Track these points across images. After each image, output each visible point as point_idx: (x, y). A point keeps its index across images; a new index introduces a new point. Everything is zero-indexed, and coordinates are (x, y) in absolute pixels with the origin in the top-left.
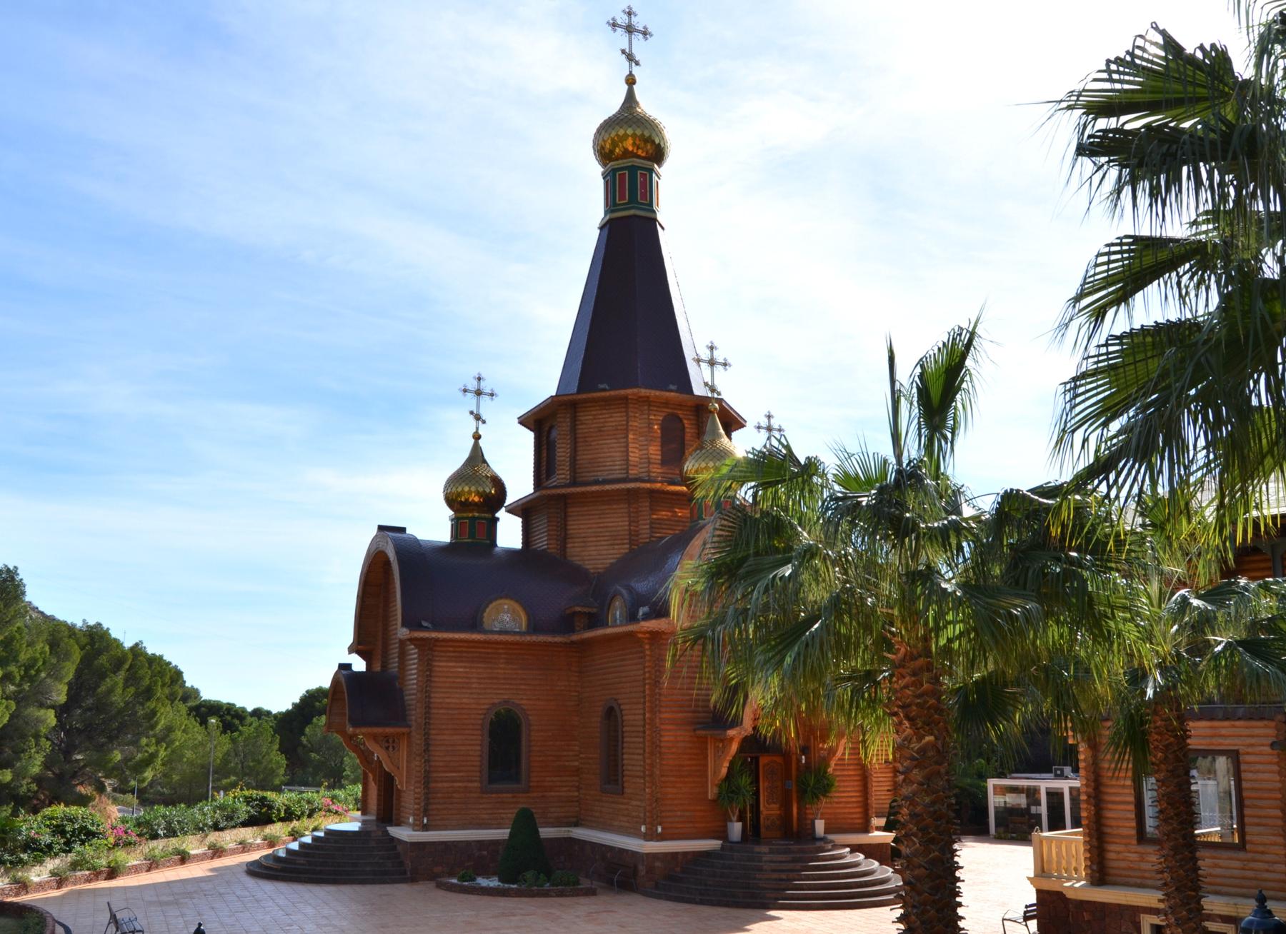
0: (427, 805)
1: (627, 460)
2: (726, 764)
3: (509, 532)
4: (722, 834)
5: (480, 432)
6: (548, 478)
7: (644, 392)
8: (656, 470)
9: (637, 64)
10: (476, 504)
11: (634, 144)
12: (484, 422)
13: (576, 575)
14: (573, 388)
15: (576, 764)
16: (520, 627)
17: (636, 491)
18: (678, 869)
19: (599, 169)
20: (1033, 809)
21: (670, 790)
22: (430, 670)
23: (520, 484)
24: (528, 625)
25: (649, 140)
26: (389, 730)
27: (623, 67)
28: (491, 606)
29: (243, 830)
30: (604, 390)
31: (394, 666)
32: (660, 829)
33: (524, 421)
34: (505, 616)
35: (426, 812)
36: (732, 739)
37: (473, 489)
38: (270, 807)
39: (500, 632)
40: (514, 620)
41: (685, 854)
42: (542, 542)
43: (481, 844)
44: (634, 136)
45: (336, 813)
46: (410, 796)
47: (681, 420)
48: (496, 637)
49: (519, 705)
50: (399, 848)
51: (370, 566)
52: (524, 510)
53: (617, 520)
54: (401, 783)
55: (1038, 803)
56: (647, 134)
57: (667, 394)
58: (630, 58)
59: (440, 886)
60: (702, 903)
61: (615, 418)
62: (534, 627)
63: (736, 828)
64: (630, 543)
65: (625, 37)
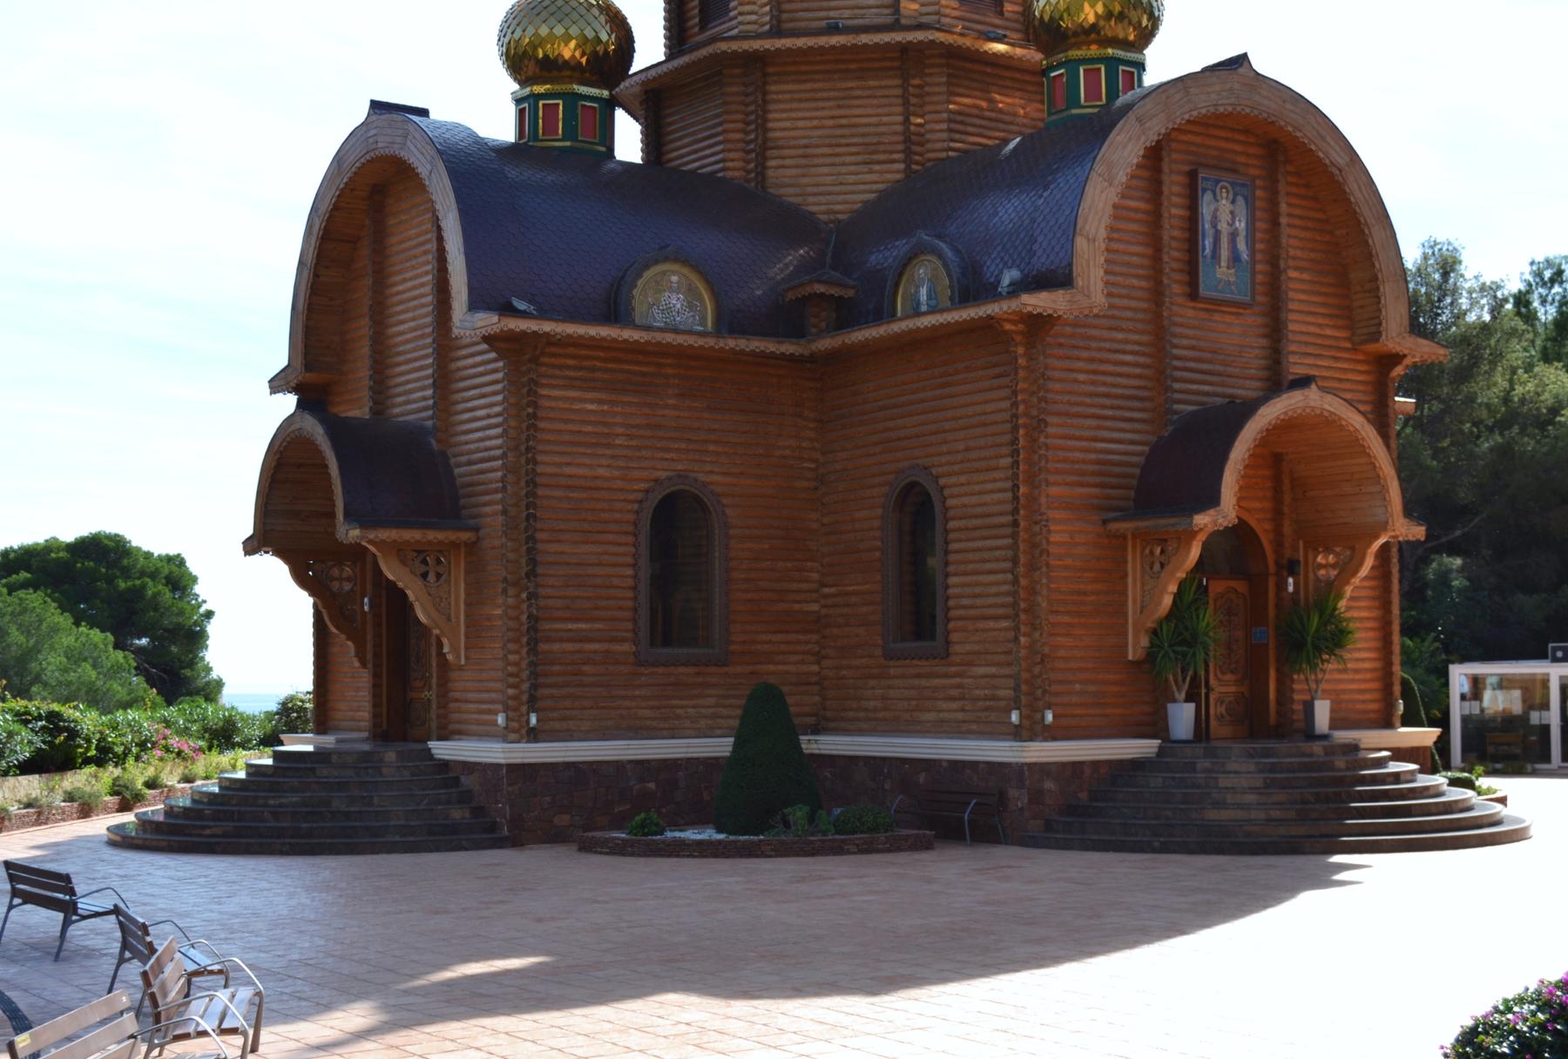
0: (535, 687)
2: (1173, 588)
4: (1156, 726)
6: (703, 26)
13: (790, 223)
15: (814, 607)
16: (703, 322)
18: (1084, 796)
20: (1535, 718)
21: (1061, 640)
22: (535, 405)
24: (718, 319)
26: (432, 535)
28: (648, 274)
29: (23, 779)
32: (1049, 717)
34: (672, 302)
35: (533, 703)
36: (1192, 534)
37: (574, 31)
38: (73, 734)
40: (691, 307)
41: (1096, 764)
42: (708, 151)
43: (644, 767)
49: (705, 484)
53: (876, 111)
55: (1545, 706)
59: (587, 847)
60: (1166, 849)
62: (729, 322)
63: (1182, 717)
64: (908, 161)
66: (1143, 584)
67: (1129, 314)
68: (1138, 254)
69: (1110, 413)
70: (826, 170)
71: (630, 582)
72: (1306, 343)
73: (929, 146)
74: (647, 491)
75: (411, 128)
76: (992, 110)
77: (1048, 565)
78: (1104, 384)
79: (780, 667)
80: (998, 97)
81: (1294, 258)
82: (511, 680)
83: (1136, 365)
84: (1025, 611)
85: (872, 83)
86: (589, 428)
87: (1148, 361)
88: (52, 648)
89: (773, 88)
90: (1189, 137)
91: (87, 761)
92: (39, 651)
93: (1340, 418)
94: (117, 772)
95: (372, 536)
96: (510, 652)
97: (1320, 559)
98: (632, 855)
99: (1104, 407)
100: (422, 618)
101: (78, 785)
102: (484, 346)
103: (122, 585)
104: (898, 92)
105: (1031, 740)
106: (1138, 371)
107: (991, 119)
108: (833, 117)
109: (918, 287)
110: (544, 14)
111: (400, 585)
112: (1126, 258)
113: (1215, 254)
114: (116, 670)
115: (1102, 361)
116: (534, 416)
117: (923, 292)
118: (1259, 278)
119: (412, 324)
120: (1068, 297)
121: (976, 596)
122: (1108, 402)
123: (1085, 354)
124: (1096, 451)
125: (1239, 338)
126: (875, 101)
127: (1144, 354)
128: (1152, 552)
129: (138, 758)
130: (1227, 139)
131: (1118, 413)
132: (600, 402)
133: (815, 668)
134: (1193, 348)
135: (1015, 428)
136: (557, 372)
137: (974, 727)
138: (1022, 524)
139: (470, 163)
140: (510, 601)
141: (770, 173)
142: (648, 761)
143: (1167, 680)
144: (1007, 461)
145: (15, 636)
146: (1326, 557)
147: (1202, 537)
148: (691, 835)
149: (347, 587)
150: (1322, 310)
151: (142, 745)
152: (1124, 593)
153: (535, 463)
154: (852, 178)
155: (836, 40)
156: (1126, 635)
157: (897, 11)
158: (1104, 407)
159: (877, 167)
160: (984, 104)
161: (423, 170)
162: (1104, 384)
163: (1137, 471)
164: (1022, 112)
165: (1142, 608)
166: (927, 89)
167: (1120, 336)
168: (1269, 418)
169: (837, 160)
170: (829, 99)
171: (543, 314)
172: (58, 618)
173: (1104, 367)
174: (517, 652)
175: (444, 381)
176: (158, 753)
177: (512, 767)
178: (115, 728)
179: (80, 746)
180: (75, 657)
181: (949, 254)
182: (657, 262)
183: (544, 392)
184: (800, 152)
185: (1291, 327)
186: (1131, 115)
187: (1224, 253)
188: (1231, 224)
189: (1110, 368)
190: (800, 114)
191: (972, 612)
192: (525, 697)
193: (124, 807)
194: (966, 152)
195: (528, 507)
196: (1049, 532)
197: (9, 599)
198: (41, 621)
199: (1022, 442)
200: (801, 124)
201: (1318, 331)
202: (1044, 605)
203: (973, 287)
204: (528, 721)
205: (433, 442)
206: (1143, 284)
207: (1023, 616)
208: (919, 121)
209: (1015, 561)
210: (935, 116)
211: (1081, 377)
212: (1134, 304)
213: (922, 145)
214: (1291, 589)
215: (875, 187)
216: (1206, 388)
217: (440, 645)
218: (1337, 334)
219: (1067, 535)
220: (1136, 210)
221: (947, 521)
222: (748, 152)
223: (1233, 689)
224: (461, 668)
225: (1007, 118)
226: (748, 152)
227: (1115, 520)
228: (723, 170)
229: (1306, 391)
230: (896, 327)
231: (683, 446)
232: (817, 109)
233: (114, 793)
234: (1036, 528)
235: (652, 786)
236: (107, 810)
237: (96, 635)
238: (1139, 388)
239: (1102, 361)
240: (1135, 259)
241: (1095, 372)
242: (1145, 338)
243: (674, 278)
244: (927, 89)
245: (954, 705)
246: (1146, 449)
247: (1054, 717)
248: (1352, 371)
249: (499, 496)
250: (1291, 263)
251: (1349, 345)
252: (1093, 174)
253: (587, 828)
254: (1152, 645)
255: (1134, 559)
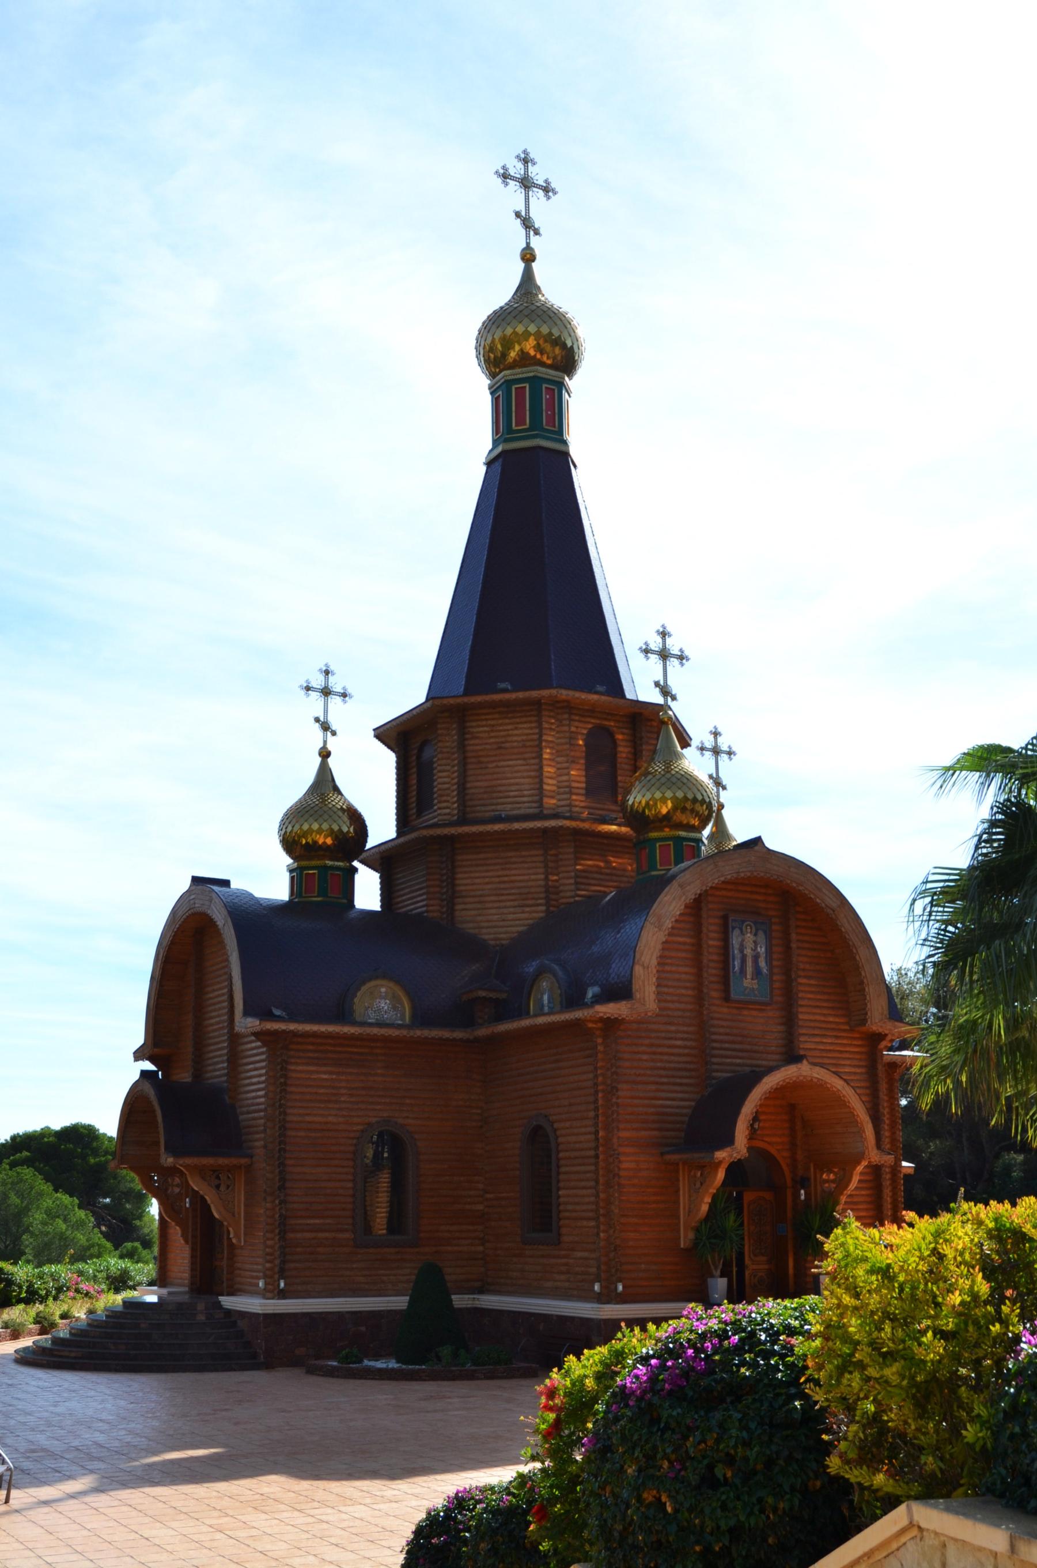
0: (283, 1262)
1: (541, 789)
2: (708, 1199)
3: (367, 891)
5: (329, 747)
6: (419, 814)
7: (564, 694)
8: (579, 800)
9: (537, 232)
10: (325, 848)
11: (538, 348)
12: (334, 733)
13: (471, 947)
14: (459, 686)
15: (480, 1207)
16: (403, 1018)
17: (556, 830)
19: (485, 382)
23: (382, 827)
24: (414, 1016)
25: (558, 342)
26: (221, 1161)
27: (518, 237)
28: (364, 988)
30: (505, 691)
31: (217, 1070)
32: (620, 1288)
33: (386, 734)
34: (381, 1004)
35: (282, 1273)
36: (720, 1162)
37: (325, 826)
39: (379, 1024)
40: (394, 1008)
42: (416, 902)
44: (538, 335)
45: (87, 1294)
46: (253, 1252)
47: (611, 735)
48: (375, 1031)
50: (241, 1324)
51: (176, 935)
52: (385, 860)
53: (527, 872)
54: (237, 1236)
56: (556, 333)
57: (595, 697)
58: (527, 224)
59: (311, 1371)
61: (520, 731)
62: (422, 1017)
65: (521, 194)
66: (690, 1196)
67: (680, 1013)
68: (686, 973)
69: (665, 1080)
70: (494, 911)
71: (351, 1192)
72: (814, 1028)
73: (562, 894)
74: (362, 1131)
75: (214, 896)
76: (608, 868)
77: (619, 1184)
78: (661, 1061)
79: (456, 1248)
80: (612, 859)
81: (804, 970)
82: (268, 1257)
83: (685, 1047)
84: (604, 1215)
85: (524, 853)
86: (322, 1091)
87: (693, 1044)
88: (38, 1208)
89: (459, 858)
90: (724, 893)
91: (20, 1301)
92: (29, 1210)
93: (826, 1083)
94: (41, 1307)
95: (181, 1162)
96: (268, 1239)
97: (824, 1176)
98: (338, 1377)
99: (661, 1076)
100: (216, 1215)
101: (13, 1317)
102: (253, 1038)
103: (92, 1161)
104: (541, 859)
105: (608, 1303)
106: (686, 1051)
107: (607, 874)
108: (499, 876)
109: (542, 994)
110: (306, 816)
111: (201, 1192)
112: (677, 976)
113: (743, 970)
114: (80, 1225)
115: (660, 1046)
116: (285, 1084)
117: (546, 997)
118: (777, 985)
119: (218, 1019)
120: (629, 1006)
121: (578, 1204)
122: (663, 1072)
123: (647, 1041)
124: (655, 1106)
125: (765, 1026)
126: (526, 865)
127: (691, 1040)
128: (695, 1176)
129: (55, 1299)
130: (752, 892)
131: (672, 1080)
132: (331, 1073)
133: (481, 1248)
134: (727, 1034)
135: (597, 1092)
136: (301, 1054)
137: (575, 1292)
138: (601, 1157)
139: (252, 918)
140: (269, 1205)
141: (457, 913)
142: (360, 1312)
143: (707, 1261)
144: (592, 1114)
145: (14, 1199)
146: (828, 1175)
147: (725, 1166)
148: (380, 1364)
149: (177, 1190)
150: (825, 1004)
151: (59, 1290)
152: (677, 1202)
153: (285, 1114)
154: (511, 916)
155: (497, 827)
156: (678, 1231)
157: (541, 806)
158: (661, 1076)
159: (527, 909)
160: (602, 864)
161: (220, 923)
162: (661, 1061)
163: (686, 1119)
164: (630, 868)
165: (690, 1212)
166: (561, 856)
167: (673, 1028)
168: (771, 1085)
169: (502, 904)
170: (495, 864)
171: (292, 1018)
172: (43, 1186)
173: (660, 1050)
174: (272, 1239)
175: (234, 1059)
176: (71, 1294)
177: (266, 1316)
178: (41, 1278)
179: (15, 1291)
180: (52, 1215)
181: (560, 973)
182: (370, 980)
183: (293, 1067)
184: (477, 899)
185: (801, 1016)
186: (675, 883)
187: (749, 970)
188: (755, 950)
189: (666, 1050)
190: (477, 875)
191: (574, 1214)
192: (277, 1269)
193: (43, 1332)
194: (589, 897)
195: (280, 1143)
196: (620, 1162)
197: (10, 1173)
198: (32, 1188)
199: (600, 1102)
200: (478, 881)
201: (823, 1019)
202: (617, 1211)
203: (573, 999)
204: (279, 1285)
205: (227, 1098)
206: (690, 992)
207: (602, 1219)
208: (555, 878)
209: (597, 1182)
210: (565, 875)
211: (645, 1057)
212: (682, 1006)
213: (557, 893)
214: (803, 1197)
215: (526, 922)
216: (738, 1061)
217: (229, 1232)
218: (837, 1020)
219: (634, 1163)
220: (685, 943)
221: (558, 1152)
222: (442, 900)
223: (766, 1267)
224: (242, 1248)
225: (619, 873)
226: (442, 900)
227: (668, 1153)
228: (427, 911)
229: (799, 1065)
230: (525, 1023)
231: (388, 1100)
232: (487, 871)
233: (36, 1322)
234: (611, 1160)
235: (363, 1329)
236: (30, 1334)
237: (66, 1199)
238: (687, 1062)
239: (660, 1046)
240: (683, 976)
241: (655, 1053)
242: (692, 1029)
243: (383, 990)
244: (561, 856)
245: (563, 1277)
246: (693, 1104)
247: (624, 1287)
248: (851, 1045)
249: (262, 1135)
250: (801, 973)
251: (847, 1027)
252: (647, 924)
253: (318, 1357)
254: (696, 1239)
255: (684, 1179)
